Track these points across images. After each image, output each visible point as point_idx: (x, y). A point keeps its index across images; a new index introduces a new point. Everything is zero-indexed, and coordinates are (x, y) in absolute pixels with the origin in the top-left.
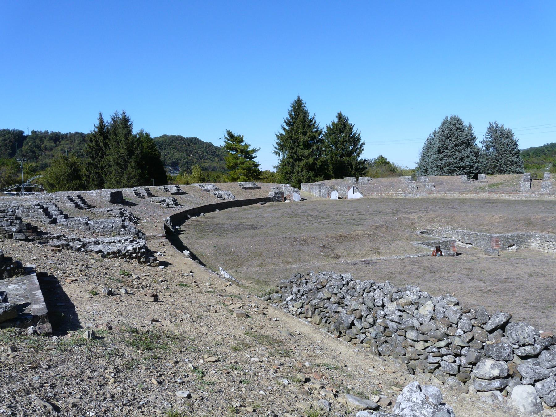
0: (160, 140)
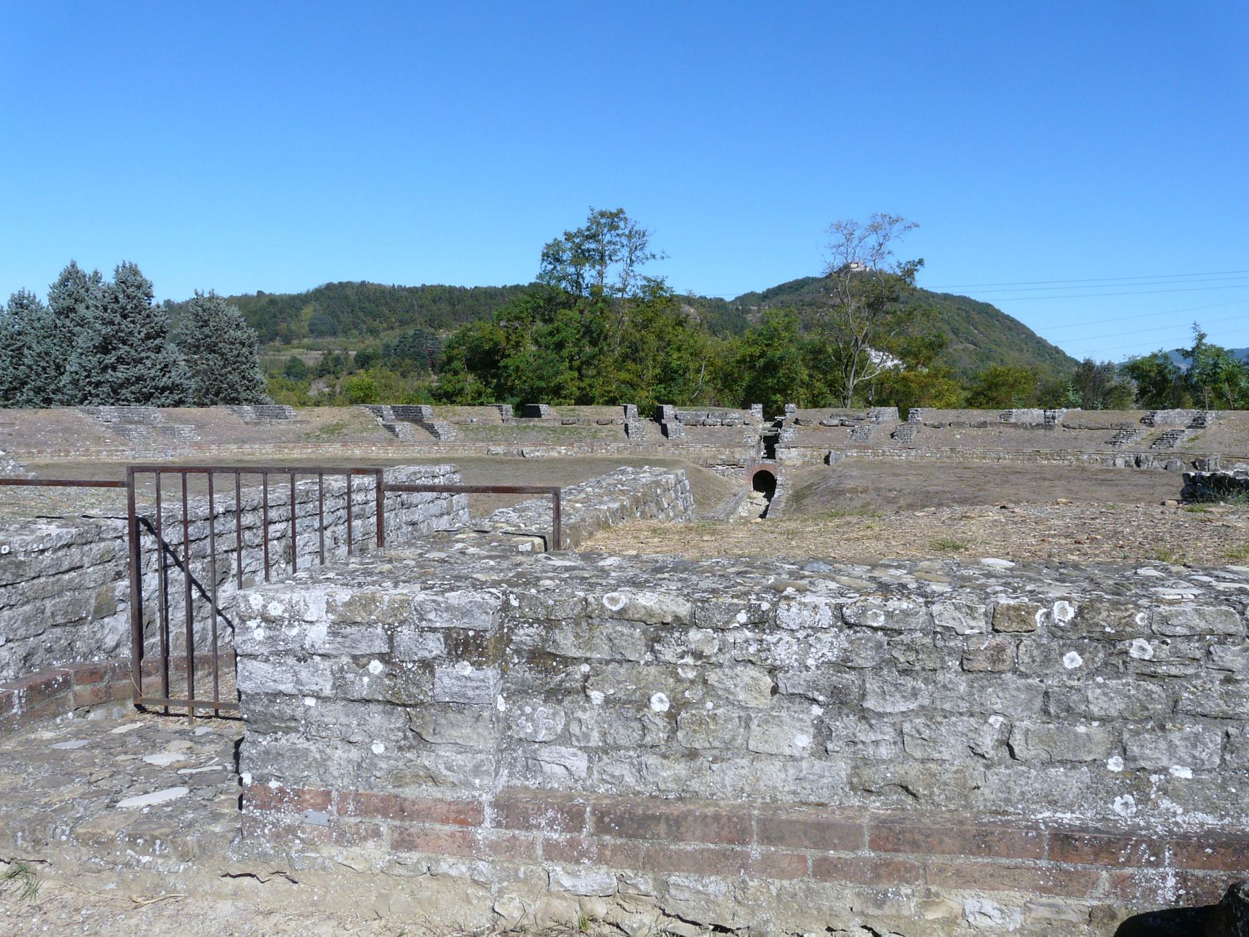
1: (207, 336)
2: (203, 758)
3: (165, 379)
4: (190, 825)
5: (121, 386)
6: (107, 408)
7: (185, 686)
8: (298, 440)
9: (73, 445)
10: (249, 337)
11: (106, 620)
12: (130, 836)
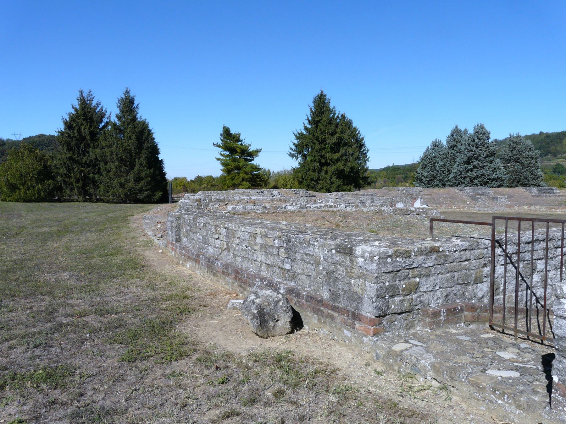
0: (36, 139)
1: (515, 155)
2: (525, 360)
3: (494, 175)
4: (522, 392)
5: (474, 178)
6: (468, 188)
7: (513, 321)
8: (560, 205)
9: (454, 204)
10: (536, 154)
11: (479, 285)
12: (493, 388)
